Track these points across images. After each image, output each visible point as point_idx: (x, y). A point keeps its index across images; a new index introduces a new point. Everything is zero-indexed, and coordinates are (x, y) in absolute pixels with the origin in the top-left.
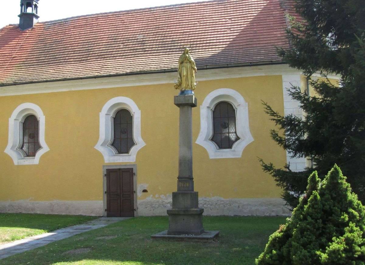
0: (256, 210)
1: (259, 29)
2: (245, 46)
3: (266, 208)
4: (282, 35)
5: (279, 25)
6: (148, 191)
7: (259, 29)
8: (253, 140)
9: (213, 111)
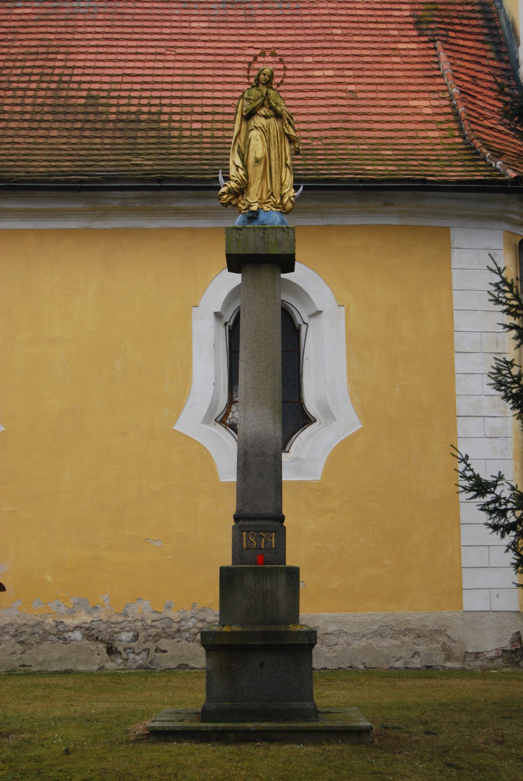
0: (366, 648)
1: (363, 88)
2: (328, 134)
3: (394, 642)
4: (439, 111)
5: (422, 81)
6: (7, 588)
7: (363, 88)
8: (360, 426)
9: (229, 326)
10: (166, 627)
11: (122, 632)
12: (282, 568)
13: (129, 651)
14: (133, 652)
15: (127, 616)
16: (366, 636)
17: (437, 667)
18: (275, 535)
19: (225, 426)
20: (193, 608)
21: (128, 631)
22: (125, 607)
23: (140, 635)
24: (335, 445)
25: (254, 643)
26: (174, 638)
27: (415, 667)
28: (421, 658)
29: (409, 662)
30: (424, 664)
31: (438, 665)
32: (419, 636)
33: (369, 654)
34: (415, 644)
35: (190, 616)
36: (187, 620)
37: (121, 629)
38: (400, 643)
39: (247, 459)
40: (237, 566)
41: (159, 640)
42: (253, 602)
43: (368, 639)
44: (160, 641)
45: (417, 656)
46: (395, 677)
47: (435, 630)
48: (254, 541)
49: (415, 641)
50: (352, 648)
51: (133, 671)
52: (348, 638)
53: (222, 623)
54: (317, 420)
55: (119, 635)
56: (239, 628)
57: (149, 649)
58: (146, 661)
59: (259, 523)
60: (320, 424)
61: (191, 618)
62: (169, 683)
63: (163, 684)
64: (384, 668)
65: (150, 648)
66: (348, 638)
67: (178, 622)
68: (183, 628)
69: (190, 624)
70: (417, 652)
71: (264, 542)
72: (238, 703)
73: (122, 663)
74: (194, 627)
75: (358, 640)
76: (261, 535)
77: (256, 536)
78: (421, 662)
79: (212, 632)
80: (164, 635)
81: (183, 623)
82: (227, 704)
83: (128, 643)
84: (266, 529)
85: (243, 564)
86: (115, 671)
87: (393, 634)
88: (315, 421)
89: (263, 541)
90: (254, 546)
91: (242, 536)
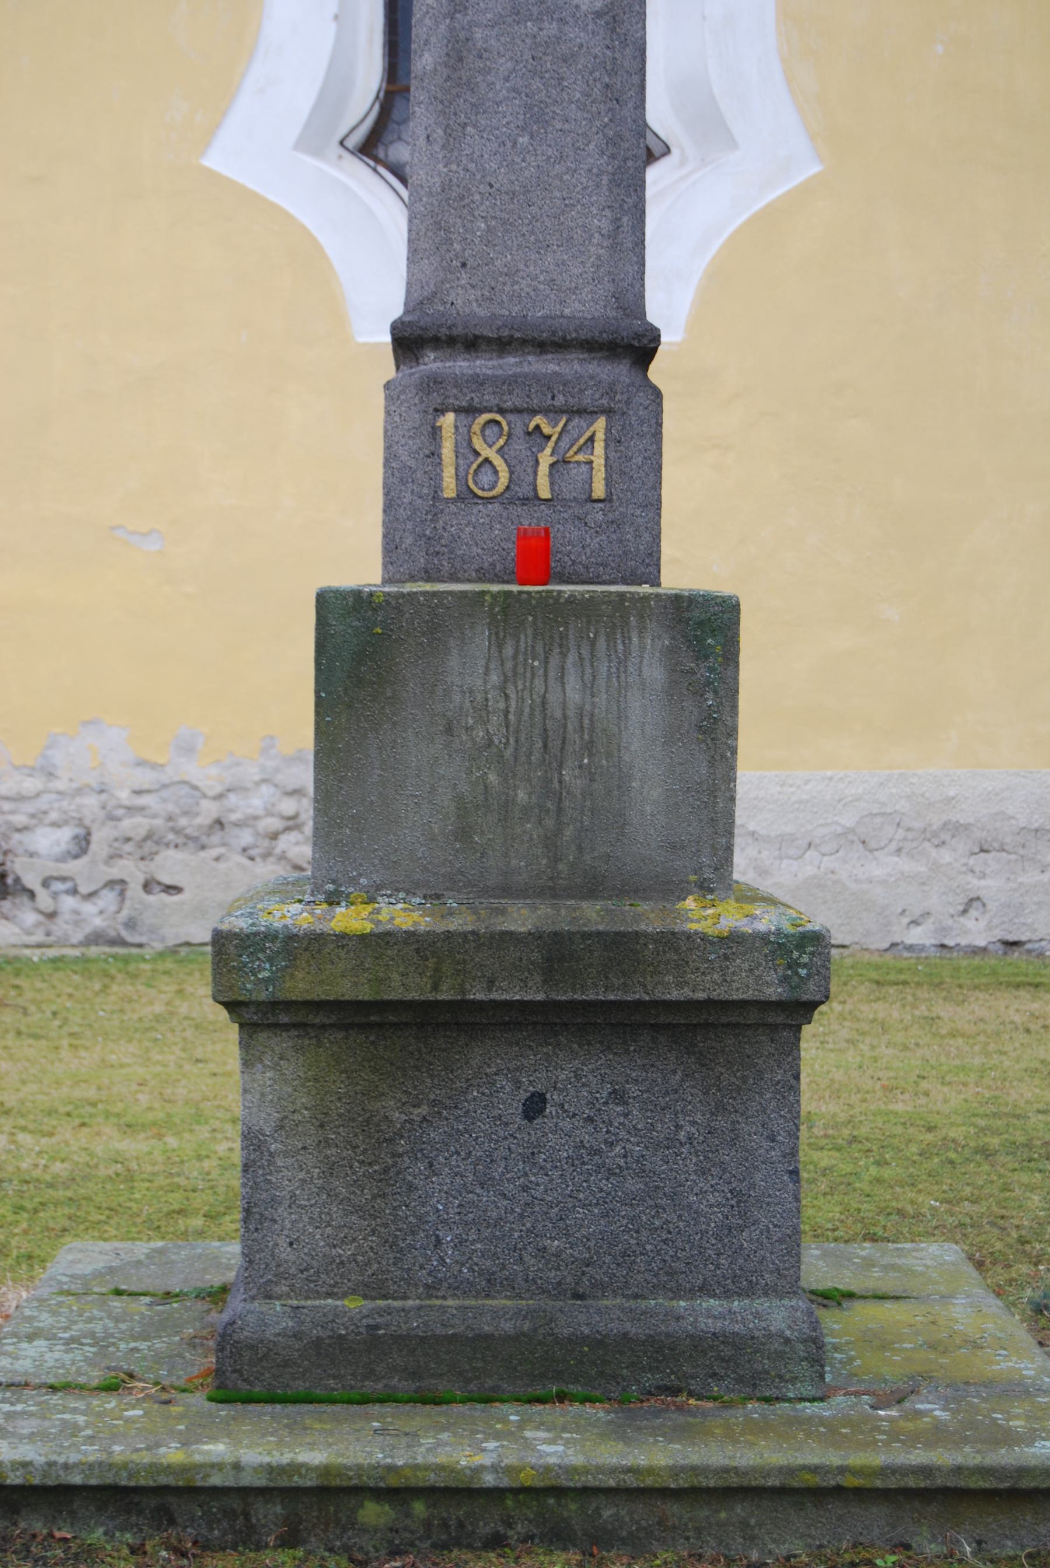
3: (906, 865)
10: (177, 811)
11: (36, 826)
12: (646, 598)
13: (58, 886)
14: (74, 892)
15: (51, 775)
16: (816, 846)
17: (1037, 945)
18: (608, 430)
19: (372, 163)
20: (265, 751)
21: (55, 825)
22: (48, 747)
23: (95, 838)
24: (731, 229)
25: (495, 996)
26: (203, 847)
27: (969, 946)
28: (987, 916)
29: (951, 929)
30: (999, 934)
31: (1041, 940)
32: (985, 847)
33: (824, 903)
34: (972, 871)
35: (257, 778)
36: (246, 789)
37: (33, 816)
38: (923, 869)
39: (462, 35)
40: (409, 588)
41: (156, 853)
42: (492, 778)
43: (824, 855)
44: (157, 858)
45: (977, 909)
46: (919, 984)
47: (1037, 831)
48: (498, 461)
49: (972, 861)
50: (774, 884)
51: (76, 952)
52: (760, 852)
53: (330, 887)
54: (672, 149)
55: (26, 838)
56: (416, 915)
57: (123, 882)
58: (114, 919)
59: (526, 369)
60: (683, 162)
61: (258, 784)
62: (177, 1002)
63: (158, 1008)
64: (873, 947)
65: (127, 879)
66: (760, 852)
67: (220, 797)
68: (234, 817)
69: (256, 803)
70: (978, 899)
71: (552, 466)
72: (410, 1303)
73: (38, 925)
74: (269, 814)
75: (791, 858)
76: (538, 427)
77: (509, 436)
78: (990, 928)
79: (270, 935)
80: (171, 836)
81: (233, 799)
82: (353, 1304)
83: (58, 860)
84: (560, 401)
85: (441, 580)
86: (14, 952)
87: (905, 839)
88: (667, 151)
89: (546, 459)
90: (500, 487)
91: (435, 432)
